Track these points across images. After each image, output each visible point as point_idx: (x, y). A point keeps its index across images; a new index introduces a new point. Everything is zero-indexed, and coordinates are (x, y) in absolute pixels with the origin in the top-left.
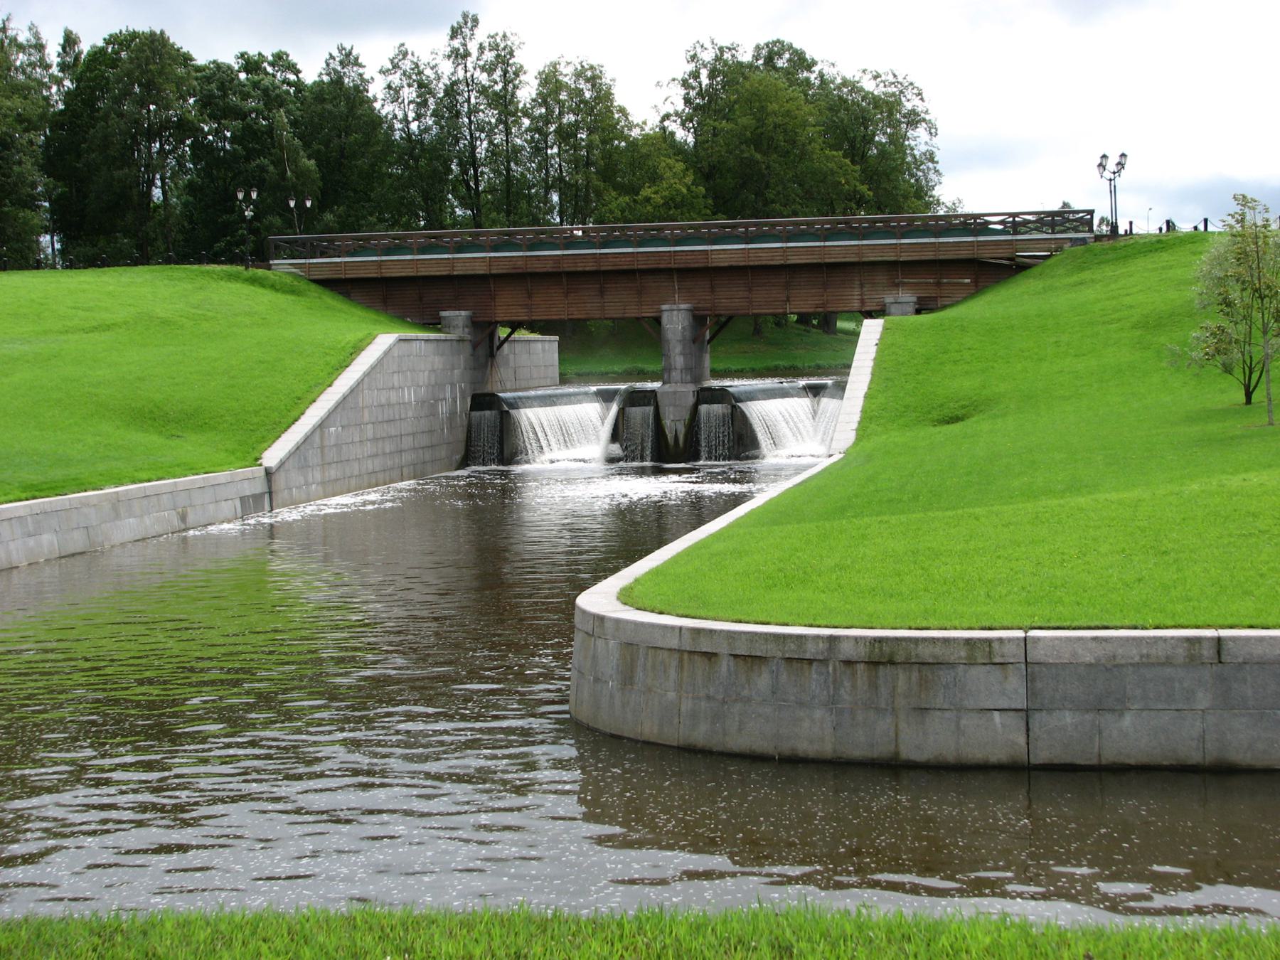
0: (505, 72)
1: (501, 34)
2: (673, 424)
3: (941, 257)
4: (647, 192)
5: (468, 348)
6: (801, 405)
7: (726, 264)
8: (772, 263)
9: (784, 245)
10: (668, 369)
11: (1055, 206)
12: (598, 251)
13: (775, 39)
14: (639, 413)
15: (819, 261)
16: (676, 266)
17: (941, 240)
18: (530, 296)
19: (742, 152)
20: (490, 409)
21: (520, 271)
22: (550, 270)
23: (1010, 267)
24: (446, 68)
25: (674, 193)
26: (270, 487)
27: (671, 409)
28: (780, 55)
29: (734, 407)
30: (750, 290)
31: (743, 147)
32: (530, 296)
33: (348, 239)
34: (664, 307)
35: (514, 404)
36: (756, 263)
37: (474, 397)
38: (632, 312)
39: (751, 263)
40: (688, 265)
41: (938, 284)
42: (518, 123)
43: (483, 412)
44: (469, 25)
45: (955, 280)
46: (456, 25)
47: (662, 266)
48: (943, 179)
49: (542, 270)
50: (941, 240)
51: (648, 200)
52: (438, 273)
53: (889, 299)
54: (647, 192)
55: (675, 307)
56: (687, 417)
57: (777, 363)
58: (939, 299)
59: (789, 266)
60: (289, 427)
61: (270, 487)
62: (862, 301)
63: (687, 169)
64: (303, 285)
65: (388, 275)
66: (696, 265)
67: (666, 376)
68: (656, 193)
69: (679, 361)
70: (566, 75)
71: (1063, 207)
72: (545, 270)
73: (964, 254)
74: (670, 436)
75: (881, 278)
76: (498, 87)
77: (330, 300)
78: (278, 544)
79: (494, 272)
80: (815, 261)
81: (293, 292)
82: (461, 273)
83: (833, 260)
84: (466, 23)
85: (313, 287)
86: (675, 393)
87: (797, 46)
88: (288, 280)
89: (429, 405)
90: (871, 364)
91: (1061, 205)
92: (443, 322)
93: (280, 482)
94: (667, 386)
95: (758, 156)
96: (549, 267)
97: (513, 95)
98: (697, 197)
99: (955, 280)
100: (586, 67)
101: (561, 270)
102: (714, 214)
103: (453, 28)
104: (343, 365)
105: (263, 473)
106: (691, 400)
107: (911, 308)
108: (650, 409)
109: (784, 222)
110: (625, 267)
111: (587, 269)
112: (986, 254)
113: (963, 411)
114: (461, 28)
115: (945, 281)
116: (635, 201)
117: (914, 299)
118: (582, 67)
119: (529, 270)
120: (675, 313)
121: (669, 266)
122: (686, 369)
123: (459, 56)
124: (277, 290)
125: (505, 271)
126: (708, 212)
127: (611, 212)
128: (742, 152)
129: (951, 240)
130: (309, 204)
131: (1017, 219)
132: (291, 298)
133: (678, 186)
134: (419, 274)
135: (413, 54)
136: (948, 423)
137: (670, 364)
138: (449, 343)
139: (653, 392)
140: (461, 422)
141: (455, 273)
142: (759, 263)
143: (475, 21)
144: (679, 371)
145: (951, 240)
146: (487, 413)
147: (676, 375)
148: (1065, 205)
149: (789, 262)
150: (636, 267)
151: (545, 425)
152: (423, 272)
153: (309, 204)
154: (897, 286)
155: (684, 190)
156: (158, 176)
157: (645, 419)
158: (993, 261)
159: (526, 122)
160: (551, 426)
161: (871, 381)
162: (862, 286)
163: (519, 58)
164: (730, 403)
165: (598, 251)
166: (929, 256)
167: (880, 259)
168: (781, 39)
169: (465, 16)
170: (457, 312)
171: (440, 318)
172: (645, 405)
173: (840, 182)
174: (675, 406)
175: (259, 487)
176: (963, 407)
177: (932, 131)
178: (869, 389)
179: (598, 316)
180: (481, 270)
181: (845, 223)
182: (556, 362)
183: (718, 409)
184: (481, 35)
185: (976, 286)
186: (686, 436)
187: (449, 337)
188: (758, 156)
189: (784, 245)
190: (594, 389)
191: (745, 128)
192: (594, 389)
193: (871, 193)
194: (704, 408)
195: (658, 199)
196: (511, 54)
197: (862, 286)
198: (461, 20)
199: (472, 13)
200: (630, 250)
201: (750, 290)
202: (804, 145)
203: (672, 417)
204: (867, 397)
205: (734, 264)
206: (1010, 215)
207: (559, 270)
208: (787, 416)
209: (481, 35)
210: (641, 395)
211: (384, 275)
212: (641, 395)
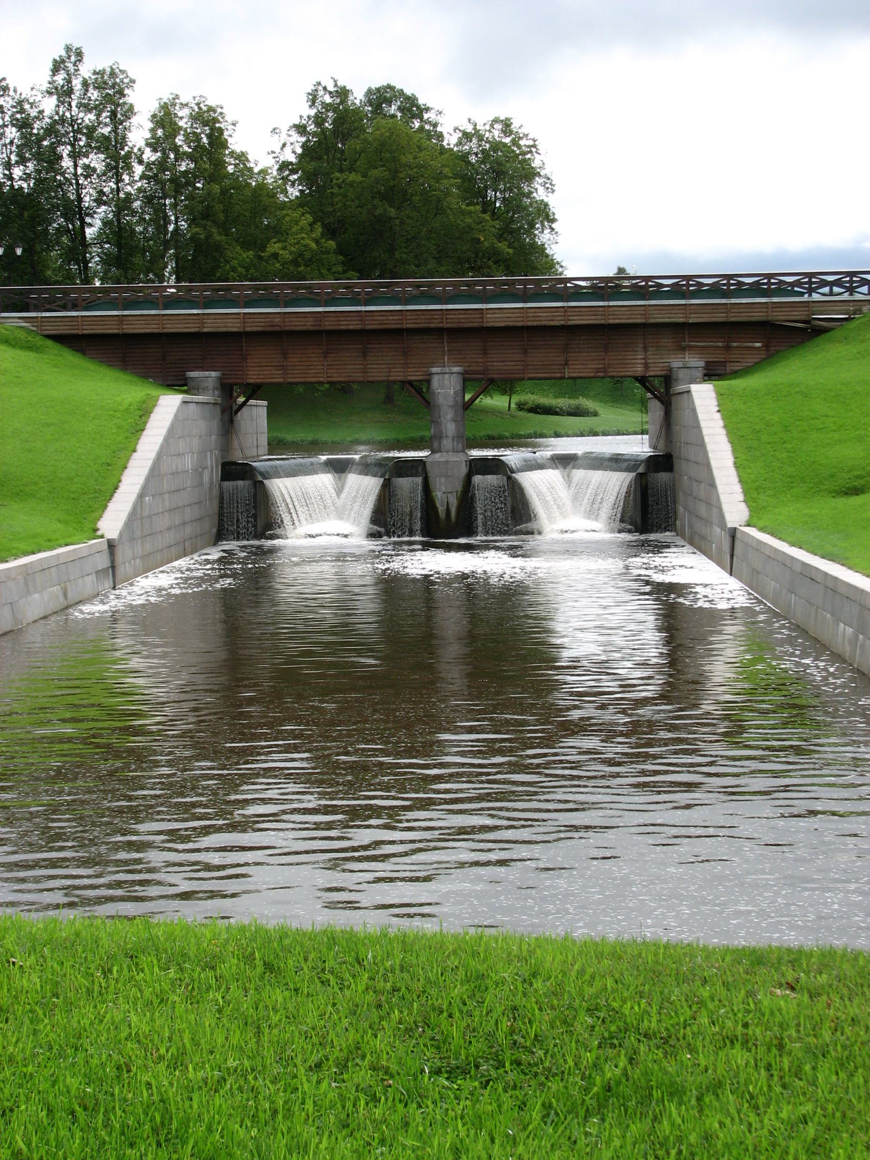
0: (114, 114)
1: (108, 70)
2: (445, 496)
3: (733, 319)
4: (274, 247)
5: (218, 410)
6: (325, 480)
7: (502, 324)
10: (439, 437)
11: (611, 272)
12: (363, 308)
13: (385, 84)
14: (407, 485)
15: (603, 322)
16: (449, 325)
17: (733, 301)
18: (285, 356)
19: (375, 207)
20: (243, 479)
21: (277, 329)
22: (311, 328)
23: (803, 330)
24: (49, 105)
25: (303, 249)
26: (113, 561)
27: (443, 480)
28: (389, 102)
29: (509, 478)
30: (525, 352)
31: (377, 202)
32: (285, 356)
33: (206, 289)
34: (434, 370)
35: (267, 475)
36: (535, 324)
37: (224, 465)
38: (397, 375)
39: (529, 324)
40: (461, 325)
41: (727, 348)
42: (129, 168)
43: (235, 483)
44: (73, 59)
45: (745, 344)
46: (58, 59)
48: (559, 239)
50: (733, 301)
51: (275, 256)
52: (186, 330)
53: (676, 364)
54: (274, 247)
55: (447, 370)
56: (460, 488)
57: (421, 433)
58: (728, 364)
59: (569, 326)
60: (112, 496)
61: (113, 561)
62: (646, 365)
63: (314, 223)
64: (39, 341)
65: (131, 331)
66: (470, 325)
67: (435, 445)
68: (284, 248)
69: (450, 428)
70: (181, 118)
71: (618, 273)
72: (305, 328)
73: (757, 316)
74: (441, 510)
75: (667, 341)
76: (106, 131)
77: (69, 356)
78: (120, 626)
81: (30, 348)
82: (211, 330)
83: (617, 321)
84: (69, 57)
85: (49, 343)
86: (447, 462)
87: (408, 92)
88: (22, 335)
89: (198, 471)
90: (723, 432)
91: (616, 271)
92: (191, 384)
93: (123, 553)
94: (438, 455)
95: (392, 212)
96: (309, 325)
97: (124, 138)
98: (328, 252)
99: (745, 344)
100: (205, 108)
101: (322, 328)
102: (345, 272)
103: (55, 60)
104: (139, 429)
105: (105, 547)
106: (464, 470)
107: (699, 374)
108: (419, 480)
109: (405, 284)
110: (393, 326)
111: (351, 327)
112: (779, 316)
113: (862, 482)
114: (63, 61)
115: (735, 344)
116: (260, 258)
117: (702, 364)
118: (200, 108)
119: (287, 328)
120: (447, 376)
121: (441, 325)
122: (458, 437)
123: (64, 93)
124: (14, 346)
125: (260, 329)
126: (340, 269)
127: (234, 269)
128: (375, 207)
130: (19, 251)
131: (569, 285)
132: (32, 355)
133: (308, 241)
134: (165, 331)
135: (15, 91)
136: (846, 494)
137: (441, 432)
138: (208, 406)
139: (421, 462)
140: (216, 492)
141: (205, 330)
142: (538, 323)
143: (79, 54)
144: (450, 440)
146: (240, 483)
147: (447, 443)
148: (621, 270)
149: (570, 323)
150: (404, 326)
152: (171, 328)
153: (19, 251)
154: (683, 349)
155: (313, 245)
157: (413, 490)
158: (788, 324)
159: (138, 170)
160: (297, 496)
161: (734, 451)
162: (645, 349)
163: (132, 97)
164: (505, 474)
165: (363, 308)
166: (720, 317)
167: (668, 320)
168: (393, 84)
169: (68, 49)
170: (207, 373)
171: (186, 379)
172: (412, 476)
173: (479, 239)
174: (447, 476)
175: (103, 562)
176: (859, 477)
177: (550, 187)
178: (736, 458)
180: (233, 327)
181: (63, 293)
182: (266, 431)
183: (492, 480)
184: (86, 70)
185: (767, 350)
186: (459, 509)
187: (200, 398)
188: (392, 212)
190: (324, 458)
191: (377, 181)
192: (324, 458)
193: (511, 251)
194: (477, 479)
195: (286, 255)
196: (122, 94)
197: (645, 349)
198: (64, 54)
199: (76, 45)
200: (195, 311)
201: (525, 352)
202: (439, 201)
203: (443, 489)
204: (737, 466)
206: (806, 275)
207: (320, 328)
209: (86, 70)
210: (410, 464)
211: (126, 331)
212: (410, 464)
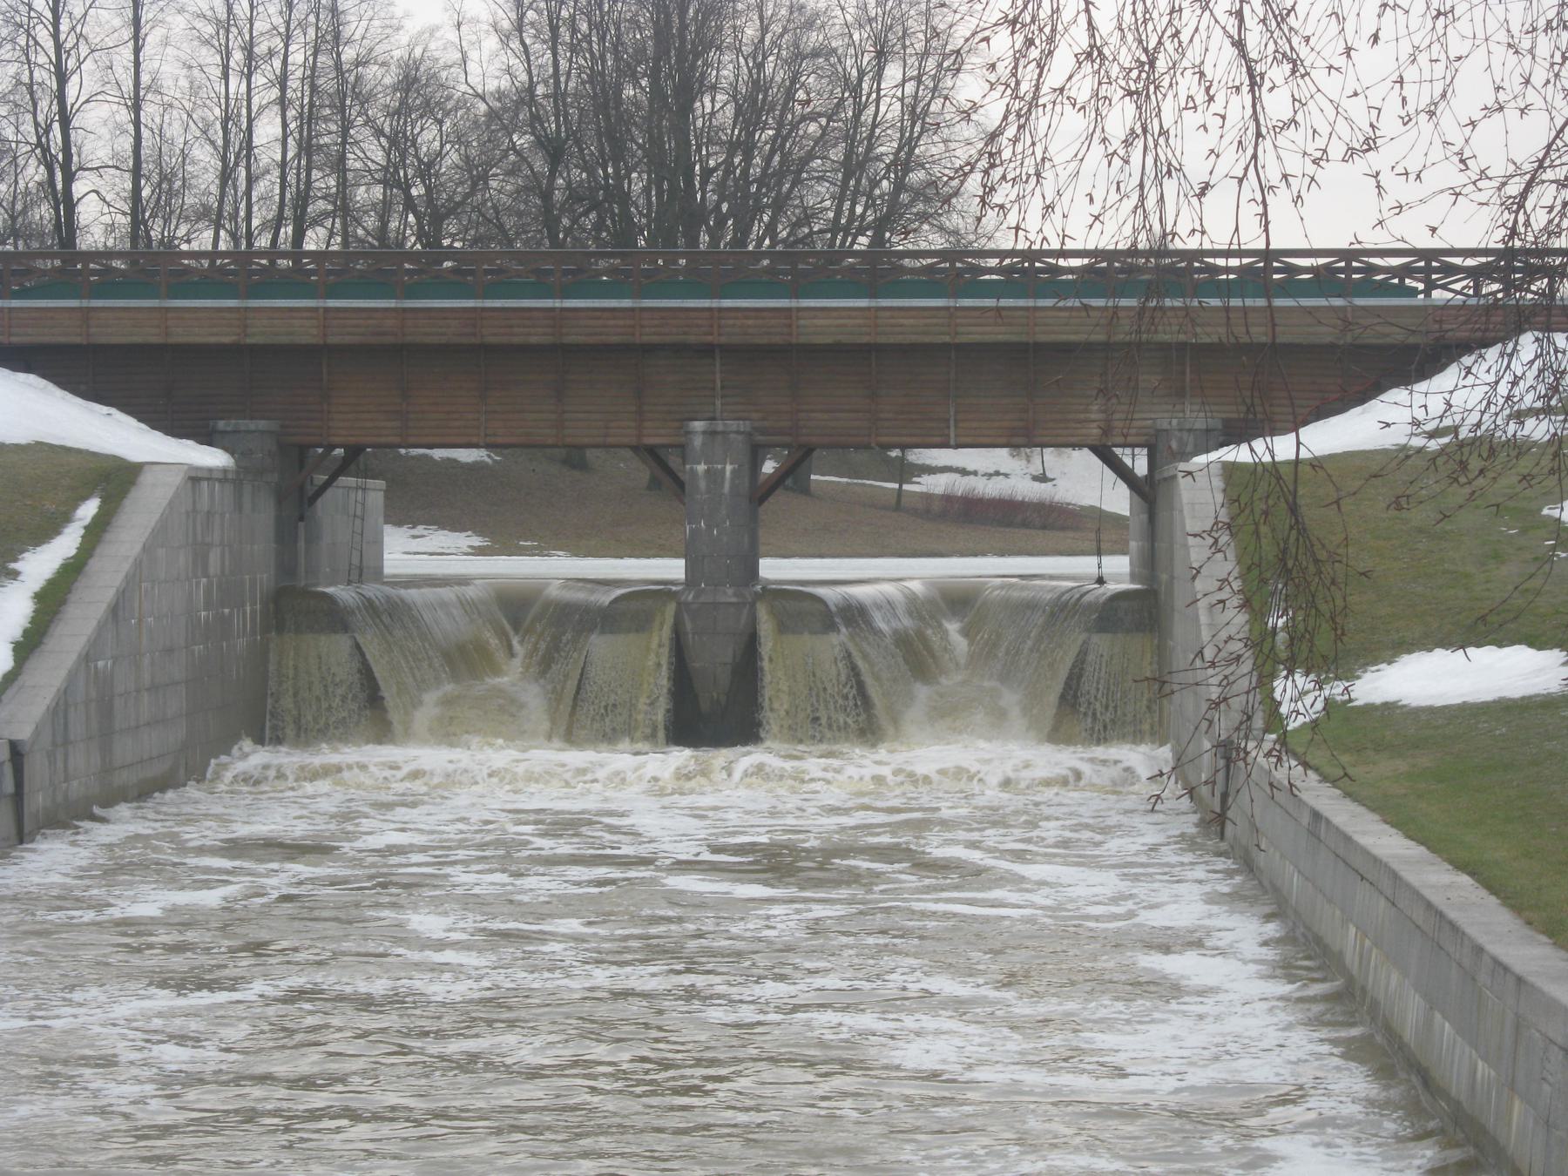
7: (829, 340)
8: (927, 339)
9: (950, 302)
12: (557, 303)
15: (1024, 338)
16: (723, 340)
21: (389, 340)
36: (892, 340)
47: (692, 339)
49: (435, 340)
52: (213, 340)
59: (959, 347)
72: (444, 340)
79: (332, 340)
80: (1001, 338)
111: (534, 340)
119: (409, 339)
121: (709, 339)
129: (498, 303)
134: (171, 340)
141: (249, 341)
145: (498, 303)
151: (568, 700)
152: (180, 336)
156: (843, 221)
165: (557, 303)
179: (550, 441)
180: (307, 334)
189: (950, 302)
205: (845, 339)
208: (225, 1021)
